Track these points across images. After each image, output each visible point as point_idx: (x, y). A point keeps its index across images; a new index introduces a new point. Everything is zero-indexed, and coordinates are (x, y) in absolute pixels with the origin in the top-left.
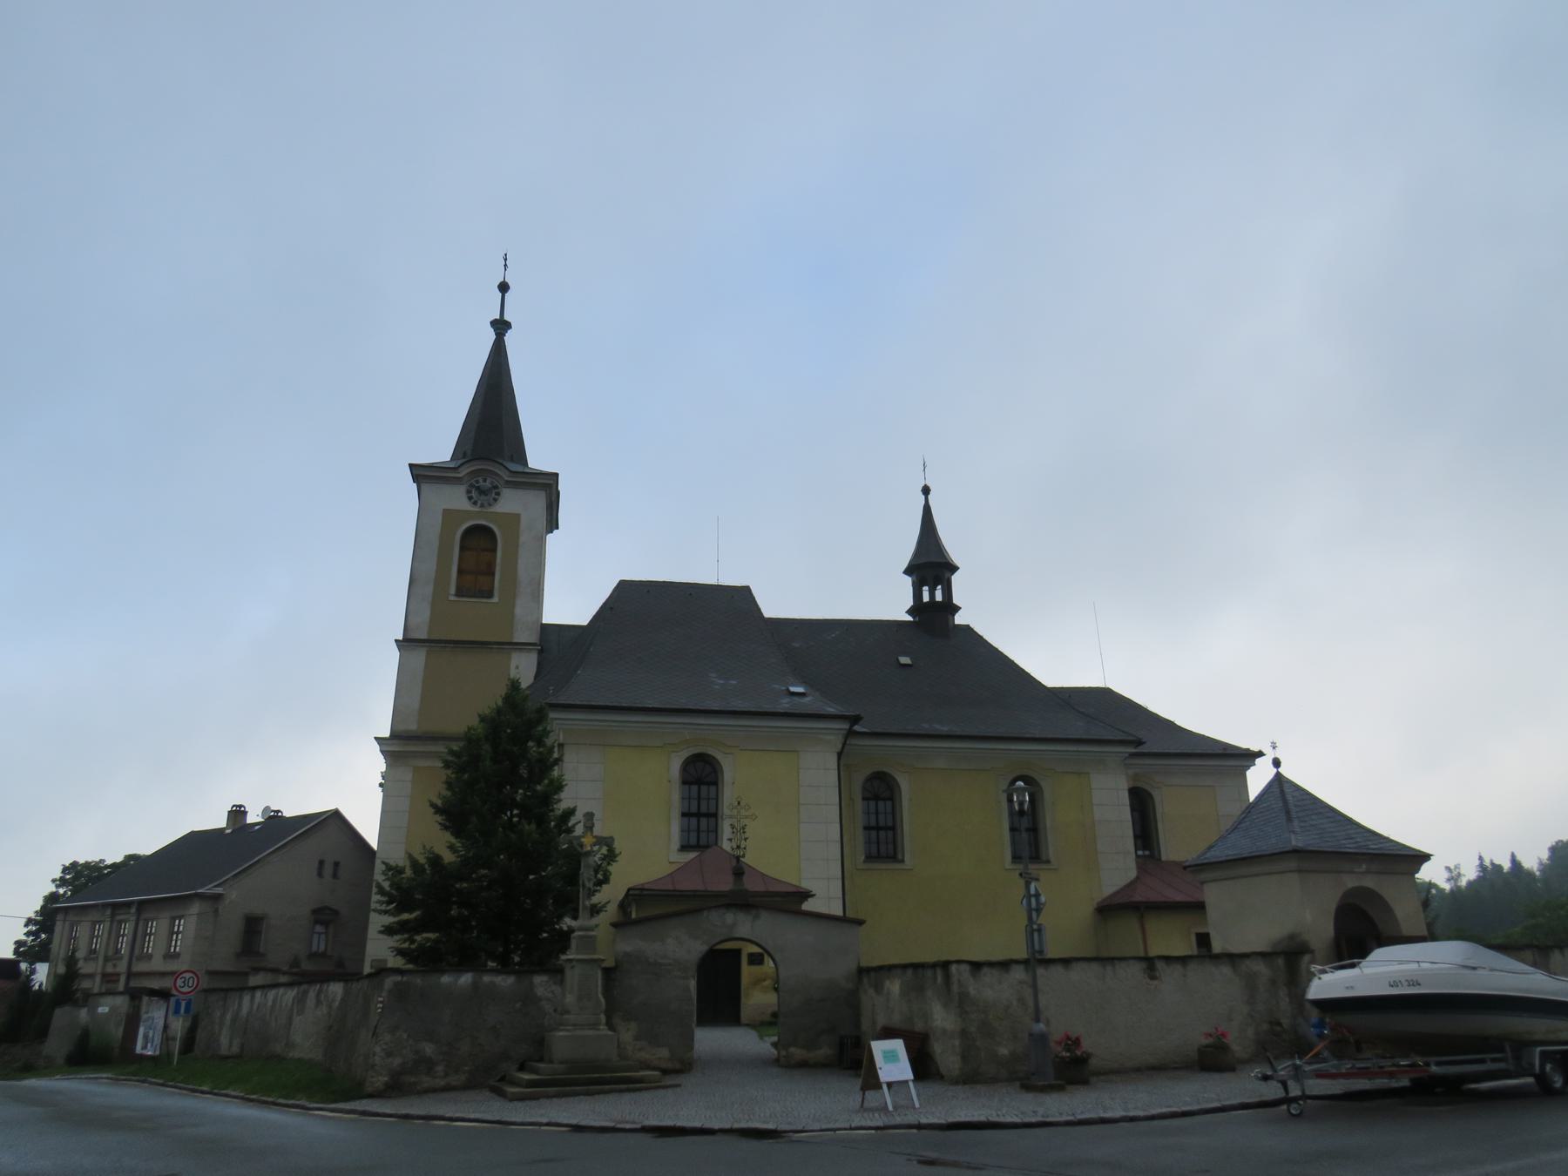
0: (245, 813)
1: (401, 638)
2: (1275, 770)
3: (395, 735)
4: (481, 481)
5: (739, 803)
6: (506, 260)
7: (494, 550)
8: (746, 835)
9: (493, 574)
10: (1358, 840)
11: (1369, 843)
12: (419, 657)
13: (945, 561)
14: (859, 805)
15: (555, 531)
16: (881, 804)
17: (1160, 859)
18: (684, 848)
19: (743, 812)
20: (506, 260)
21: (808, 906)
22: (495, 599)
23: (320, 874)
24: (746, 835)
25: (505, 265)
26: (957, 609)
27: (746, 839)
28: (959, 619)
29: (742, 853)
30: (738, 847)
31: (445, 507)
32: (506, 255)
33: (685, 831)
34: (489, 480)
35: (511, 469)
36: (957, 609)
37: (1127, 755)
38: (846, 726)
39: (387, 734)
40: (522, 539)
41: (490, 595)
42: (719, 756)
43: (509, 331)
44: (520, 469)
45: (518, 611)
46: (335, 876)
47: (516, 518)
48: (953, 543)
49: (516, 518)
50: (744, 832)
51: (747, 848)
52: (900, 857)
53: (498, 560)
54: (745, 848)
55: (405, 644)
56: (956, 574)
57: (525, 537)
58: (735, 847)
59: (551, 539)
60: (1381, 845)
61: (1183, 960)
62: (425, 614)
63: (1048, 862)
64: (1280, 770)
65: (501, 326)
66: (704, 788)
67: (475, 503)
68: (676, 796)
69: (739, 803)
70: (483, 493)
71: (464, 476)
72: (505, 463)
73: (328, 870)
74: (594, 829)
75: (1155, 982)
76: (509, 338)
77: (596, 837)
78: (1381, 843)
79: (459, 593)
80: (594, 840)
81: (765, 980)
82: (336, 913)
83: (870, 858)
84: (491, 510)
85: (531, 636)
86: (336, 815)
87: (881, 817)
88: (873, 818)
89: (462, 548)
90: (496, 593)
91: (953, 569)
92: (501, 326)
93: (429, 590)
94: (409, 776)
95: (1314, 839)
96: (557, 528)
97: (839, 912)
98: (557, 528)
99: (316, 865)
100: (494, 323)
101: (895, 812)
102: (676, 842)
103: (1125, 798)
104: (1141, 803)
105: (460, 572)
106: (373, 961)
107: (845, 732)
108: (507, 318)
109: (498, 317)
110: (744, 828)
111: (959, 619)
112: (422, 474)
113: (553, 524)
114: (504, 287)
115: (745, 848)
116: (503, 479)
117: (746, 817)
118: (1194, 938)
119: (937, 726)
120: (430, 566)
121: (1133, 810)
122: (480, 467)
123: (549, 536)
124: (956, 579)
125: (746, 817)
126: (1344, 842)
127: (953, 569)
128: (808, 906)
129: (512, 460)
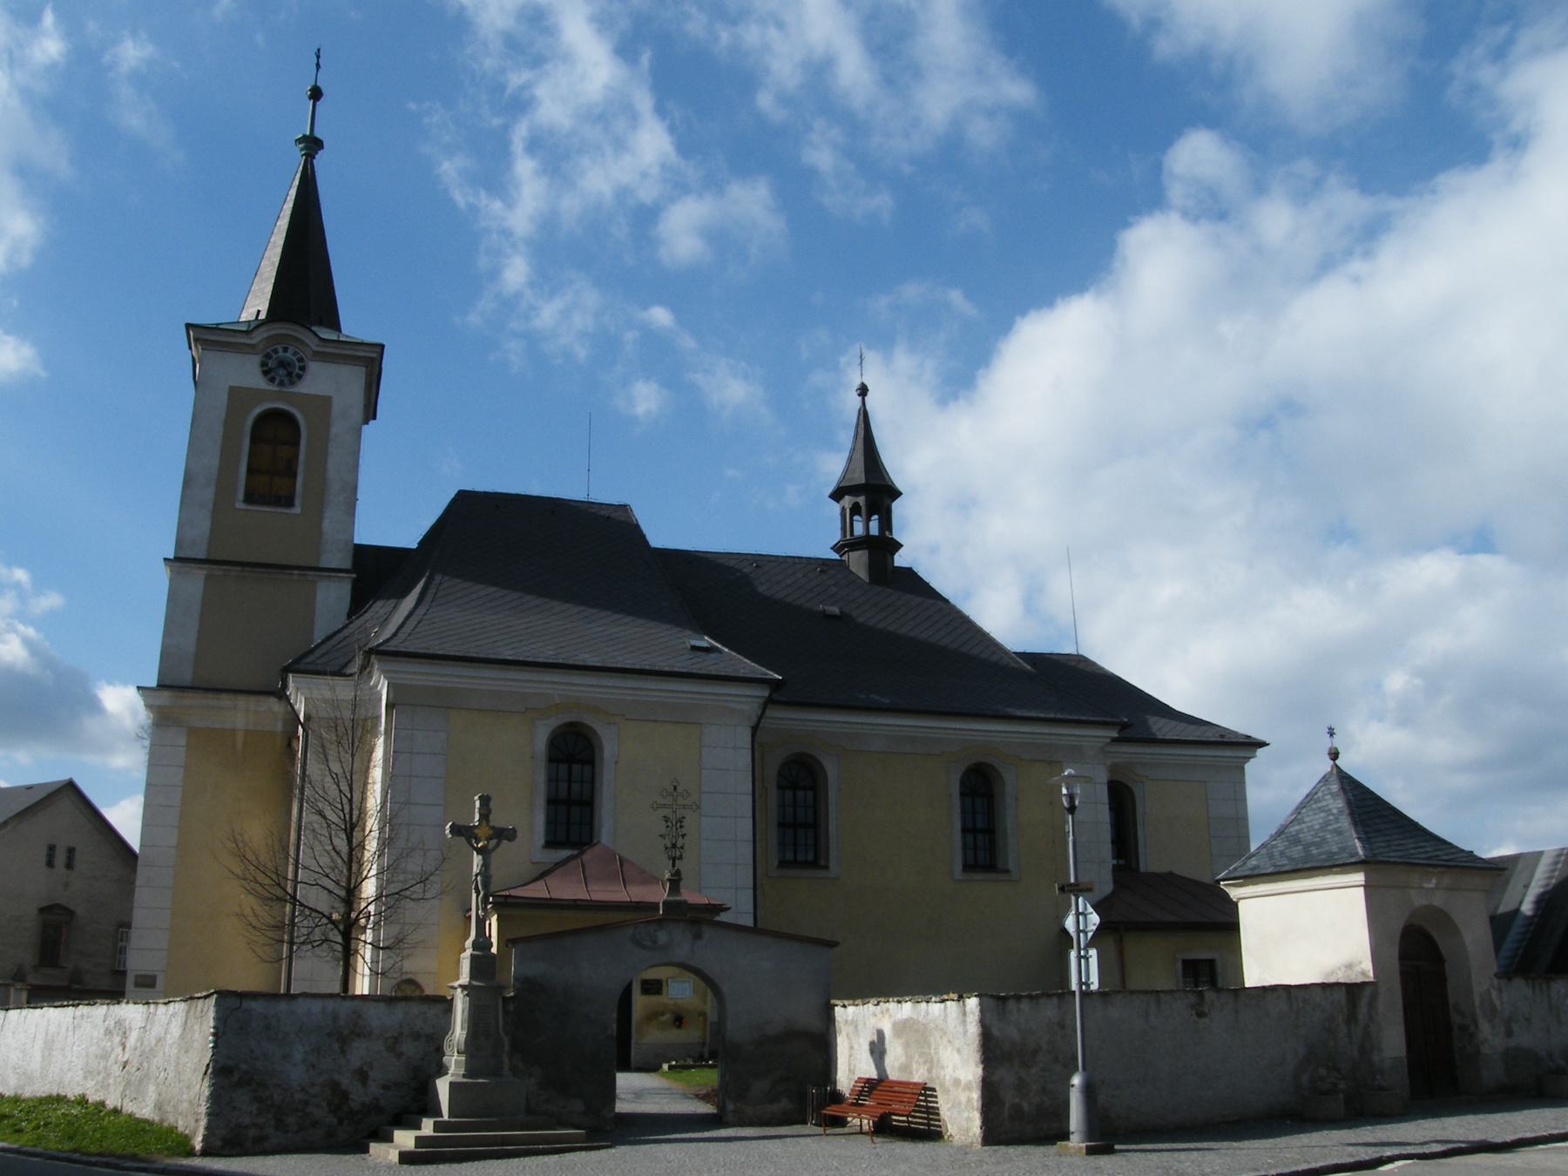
0: (509, 840)
1: (172, 557)
2: (1332, 762)
3: (161, 686)
4: (280, 350)
5: (675, 788)
6: (318, 57)
7: (297, 443)
8: (684, 831)
9: (295, 476)
10: (1429, 849)
11: (1439, 853)
12: (196, 580)
13: (884, 483)
14: (773, 795)
15: (372, 422)
16: (800, 794)
17: (1137, 870)
18: (551, 843)
19: (680, 801)
20: (318, 57)
21: (724, 917)
22: (297, 510)
23: (50, 864)
24: (684, 831)
25: (318, 65)
26: (898, 546)
27: (683, 836)
28: (900, 560)
29: (678, 854)
30: (674, 846)
31: (232, 384)
32: (319, 50)
33: (551, 822)
34: (291, 350)
35: (321, 336)
36: (898, 546)
37: (1109, 740)
38: (766, 693)
39: (154, 684)
40: (334, 430)
41: (289, 502)
42: (598, 727)
43: (320, 152)
44: (333, 337)
45: (327, 525)
46: (69, 865)
47: (326, 402)
48: (900, 465)
49: (326, 402)
50: (681, 827)
51: (686, 847)
52: (822, 862)
53: (302, 457)
54: (682, 848)
55: (179, 562)
56: (895, 502)
57: (338, 428)
58: (669, 845)
59: (369, 431)
60: (1452, 857)
61: (1171, 992)
62: (204, 525)
63: (1007, 871)
64: (1337, 762)
65: (312, 145)
66: (576, 768)
67: (272, 380)
68: (541, 778)
69: (675, 788)
70: (282, 369)
71: (259, 342)
72: (313, 328)
73: (60, 859)
74: (491, 817)
75: (1205, 1020)
76: (320, 161)
77: (493, 828)
78: (1453, 854)
79: (250, 498)
80: (491, 832)
81: (663, 1014)
82: (71, 913)
83: (783, 864)
84: (291, 390)
85: (337, 558)
86: (70, 787)
87: (576, 787)
88: (563, 787)
89: (255, 439)
90: (298, 501)
91: (895, 494)
92: (312, 145)
93: (209, 494)
94: (182, 741)
95: (1381, 847)
96: (374, 418)
97: (749, 922)
98: (374, 418)
99: (44, 851)
100: (304, 139)
101: (592, 782)
102: (540, 838)
103: (1103, 794)
104: (1121, 799)
105: (251, 471)
106: (137, 977)
107: (762, 701)
108: (318, 134)
109: (308, 133)
110: (681, 822)
111: (900, 560)
112: (207, 338)
113: (370, 413)
114: (316, 94)
115: (682, 848)
116: (311, 348)
117: (684, 807)
118: (1179, 965)
119: (875, 697)
120: (212, 461)
121: (1111, 809)
122: (283, 331)
123: (365, 427)
124: (896, 506)
125: (684, 807)
126: (1412, 851)
127: (895, 494)
128: (724, 917)
129: (321, 323)
